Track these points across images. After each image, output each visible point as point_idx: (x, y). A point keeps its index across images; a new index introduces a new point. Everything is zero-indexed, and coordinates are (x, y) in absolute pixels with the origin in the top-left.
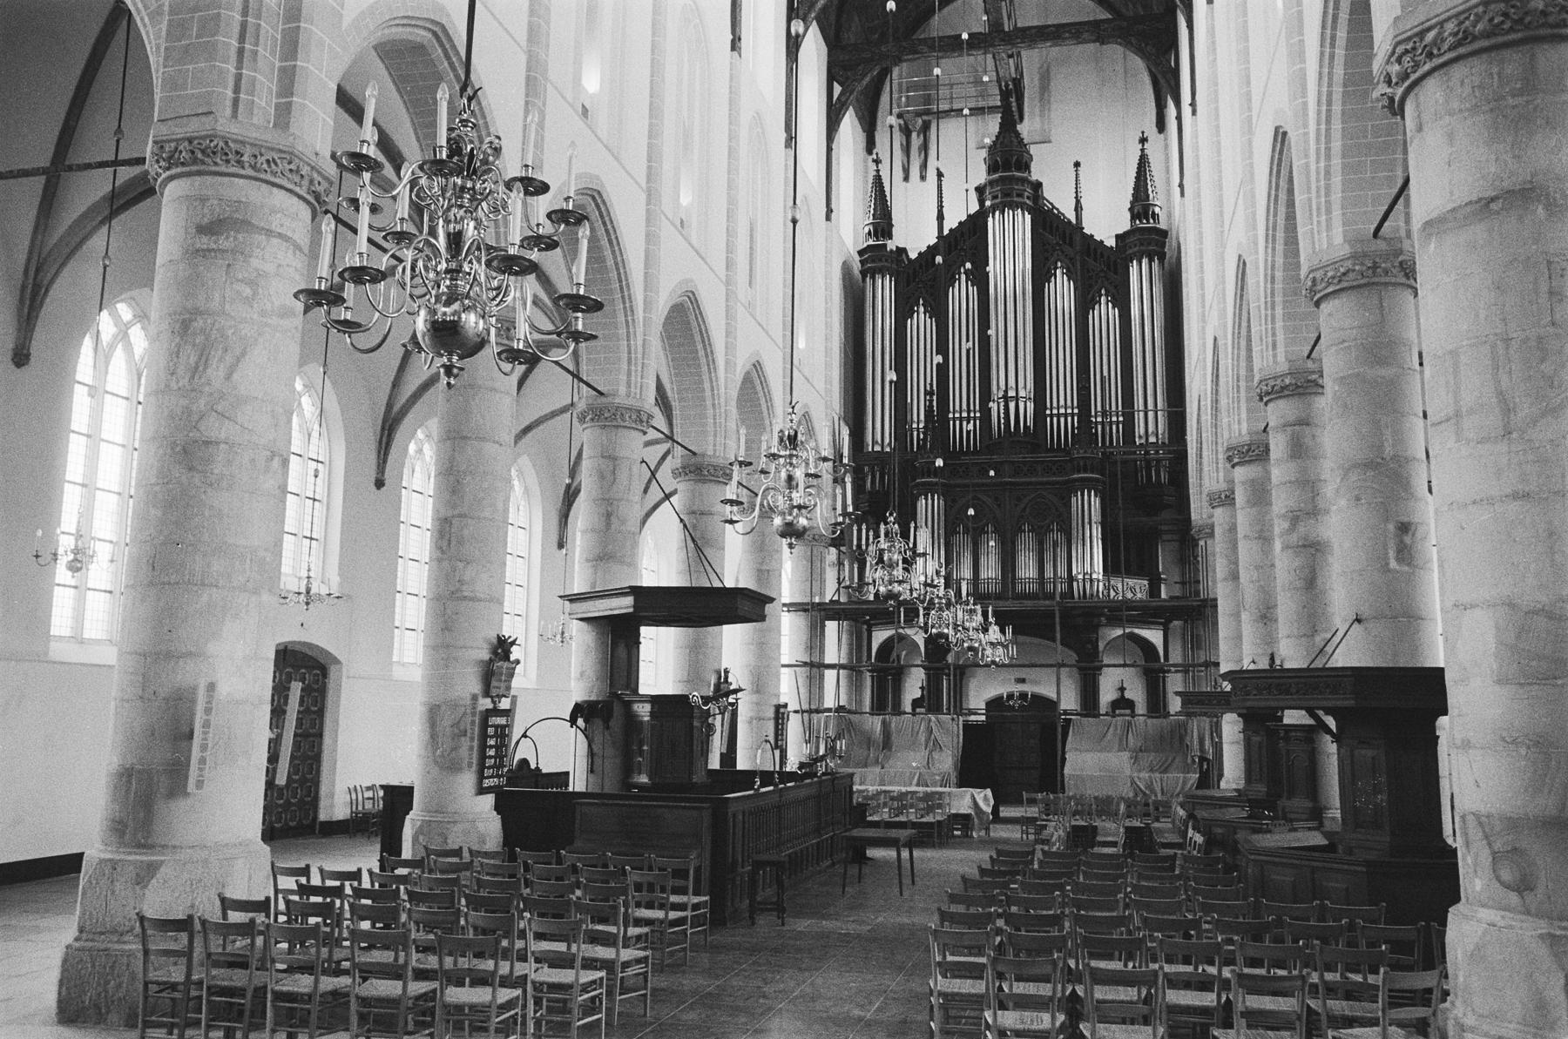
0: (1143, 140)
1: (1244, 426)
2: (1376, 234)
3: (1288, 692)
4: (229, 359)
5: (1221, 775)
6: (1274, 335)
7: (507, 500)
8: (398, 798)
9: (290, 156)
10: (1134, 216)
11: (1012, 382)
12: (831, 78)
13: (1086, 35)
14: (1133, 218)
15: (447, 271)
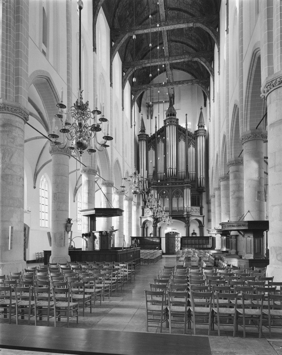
0: (201, 109)
1: (223, 173)
2: (256, 128)
3: (234, 226)
4: (10, 156)
6: (232, 152)
7: (68, 189)
8: (47, 254)
9: (20, 108)
12: (132, 94)
13: (189, 83)
15: (79, 131)
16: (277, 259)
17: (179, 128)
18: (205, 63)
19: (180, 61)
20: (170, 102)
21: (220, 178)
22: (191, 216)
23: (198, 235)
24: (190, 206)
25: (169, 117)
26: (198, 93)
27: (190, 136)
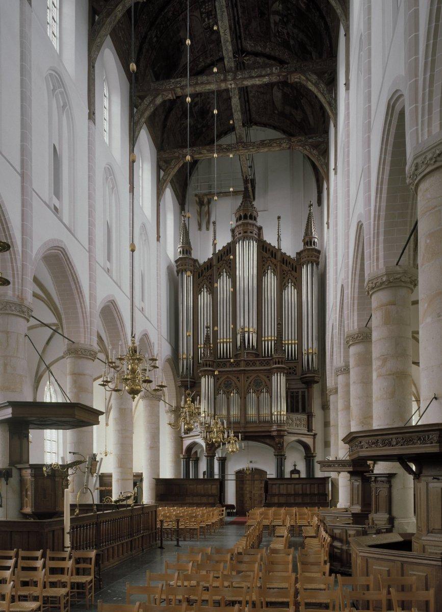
0: (310, 206)
5: (338, 502)
6: (378, 253)
10: (306, 243)
11: (246, 324)
14: (304, 245)
16: (8, 345)
17: (264, 248)
18: (316, 85)
19: (261, 83)
20: (244, 194)
21: (347, 337)
22: (286, 433)
23: (303, 475)
24: (284, 412)
25: (240, 222)
26: (304, 180)
27: (287, 264)
